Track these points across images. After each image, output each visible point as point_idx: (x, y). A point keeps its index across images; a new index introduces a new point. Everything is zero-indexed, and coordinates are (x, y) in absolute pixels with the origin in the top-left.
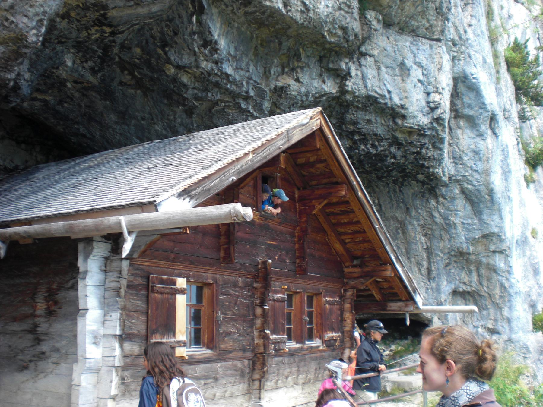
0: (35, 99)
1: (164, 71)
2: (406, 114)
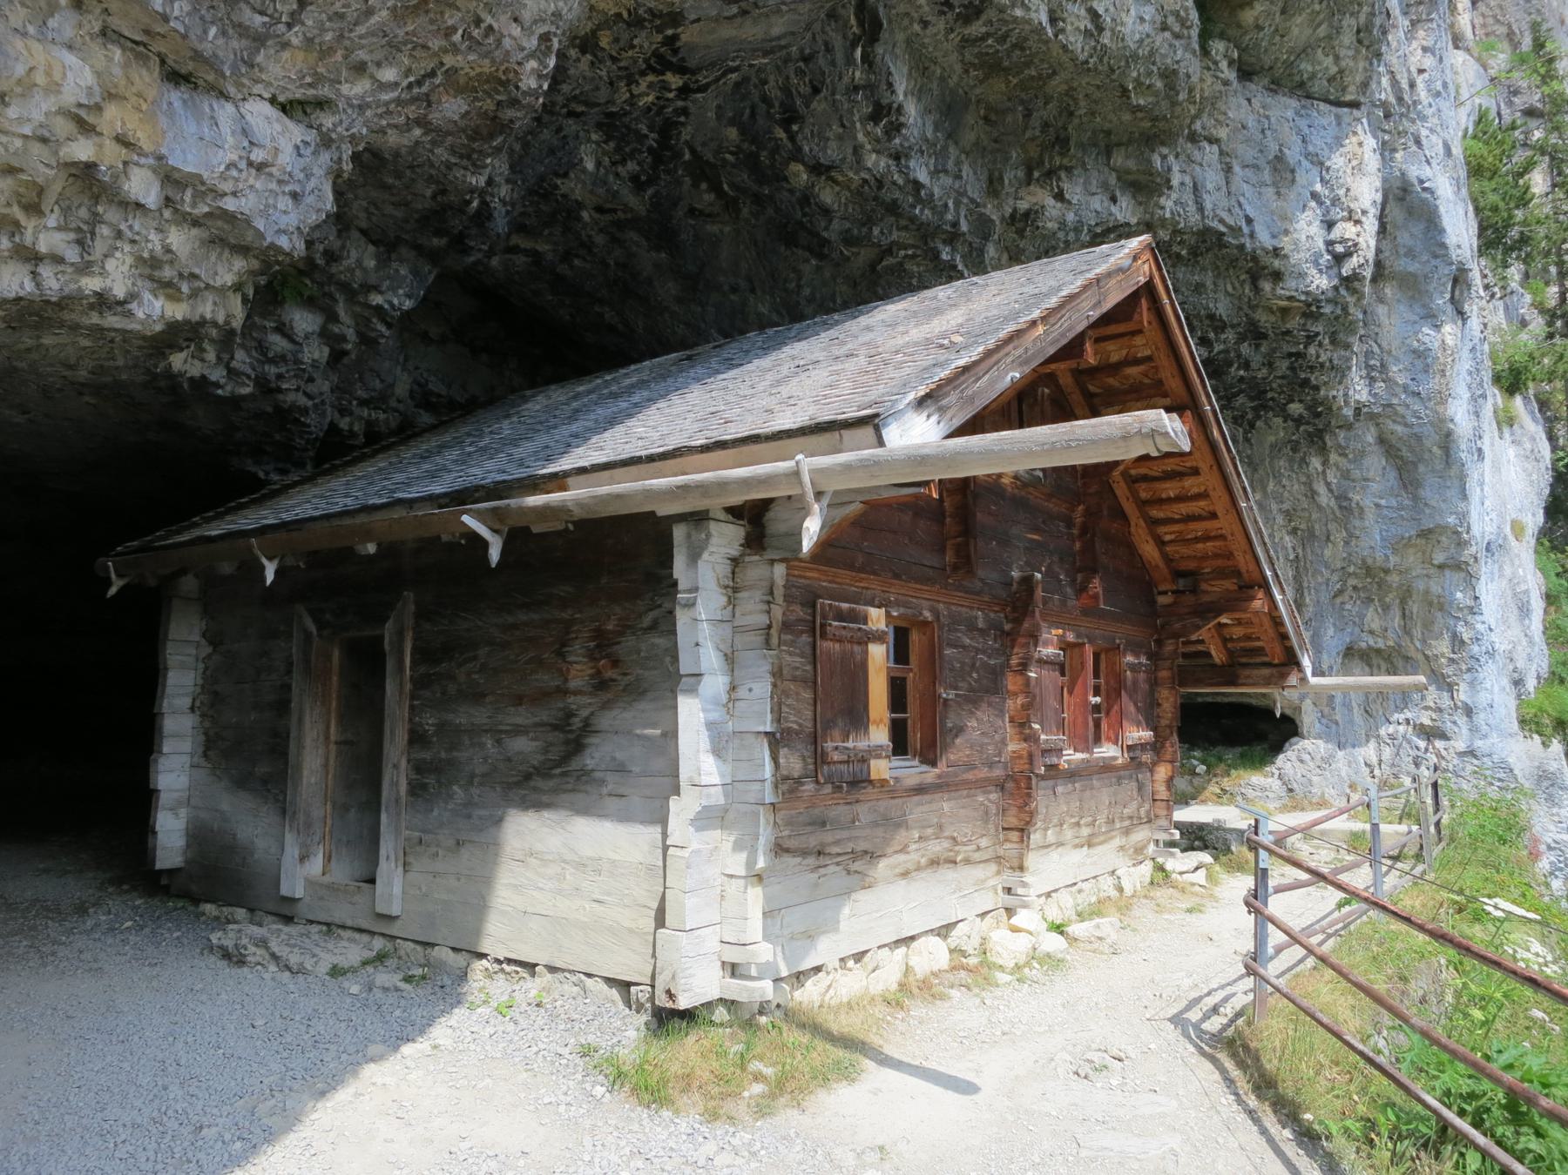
0: (514, 250)
1: (786, 179)
2: (1283, 269)
